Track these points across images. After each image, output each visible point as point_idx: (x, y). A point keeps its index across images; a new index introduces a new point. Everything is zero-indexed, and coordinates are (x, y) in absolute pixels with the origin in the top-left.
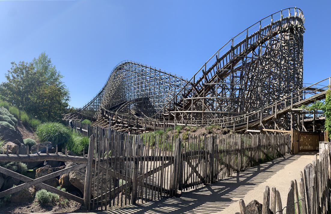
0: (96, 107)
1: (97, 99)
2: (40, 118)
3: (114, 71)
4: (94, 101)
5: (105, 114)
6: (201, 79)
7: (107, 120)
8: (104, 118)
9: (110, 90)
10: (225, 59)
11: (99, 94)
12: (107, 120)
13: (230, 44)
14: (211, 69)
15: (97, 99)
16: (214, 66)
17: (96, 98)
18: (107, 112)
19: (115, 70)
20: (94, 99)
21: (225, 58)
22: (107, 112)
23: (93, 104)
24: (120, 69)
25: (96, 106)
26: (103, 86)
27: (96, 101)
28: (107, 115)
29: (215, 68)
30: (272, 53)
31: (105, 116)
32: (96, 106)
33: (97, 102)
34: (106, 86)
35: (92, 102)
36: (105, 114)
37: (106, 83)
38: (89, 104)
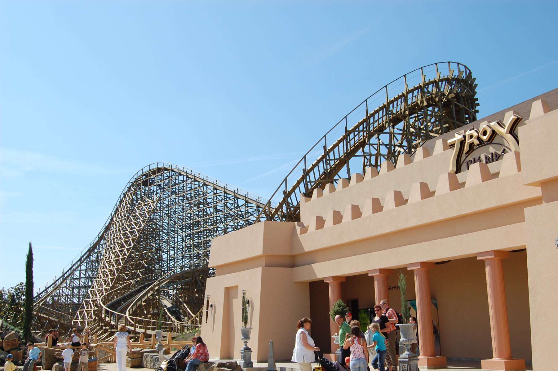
0: (79, 292)
1: (83, 267)
2: (380, 368)
3: (129, 188)
4: (72, 273)
5: (103, 316)
6: (281, 205)
7: (107, 328)
8: (103, 324)
9: (118, 243)
10: (336, 149)
11: (90, 252)
12: (107, 328)
13: (302, 166)
14: (294, 188)
15: (83, 267)
16: (299, 183)
17: (80, 266)
18: (107, 312)
19: (133, 185)
20: (72, 270)
21: (342, 143)
22: (107, 312)
23: (68, 282)
24: (146, 183)
25: (79, 290)
26: (100, 228)
27: (77, 273)
28: (107, 319)
29: (302, 185)
30: (185, 305)
31: (102, 320)
32: (79, 290)
33: (82, 276)
34: (107, 228)
35: (68, 276)
36: (103, 316)
37: (109, 221)
38: (58, 283)
